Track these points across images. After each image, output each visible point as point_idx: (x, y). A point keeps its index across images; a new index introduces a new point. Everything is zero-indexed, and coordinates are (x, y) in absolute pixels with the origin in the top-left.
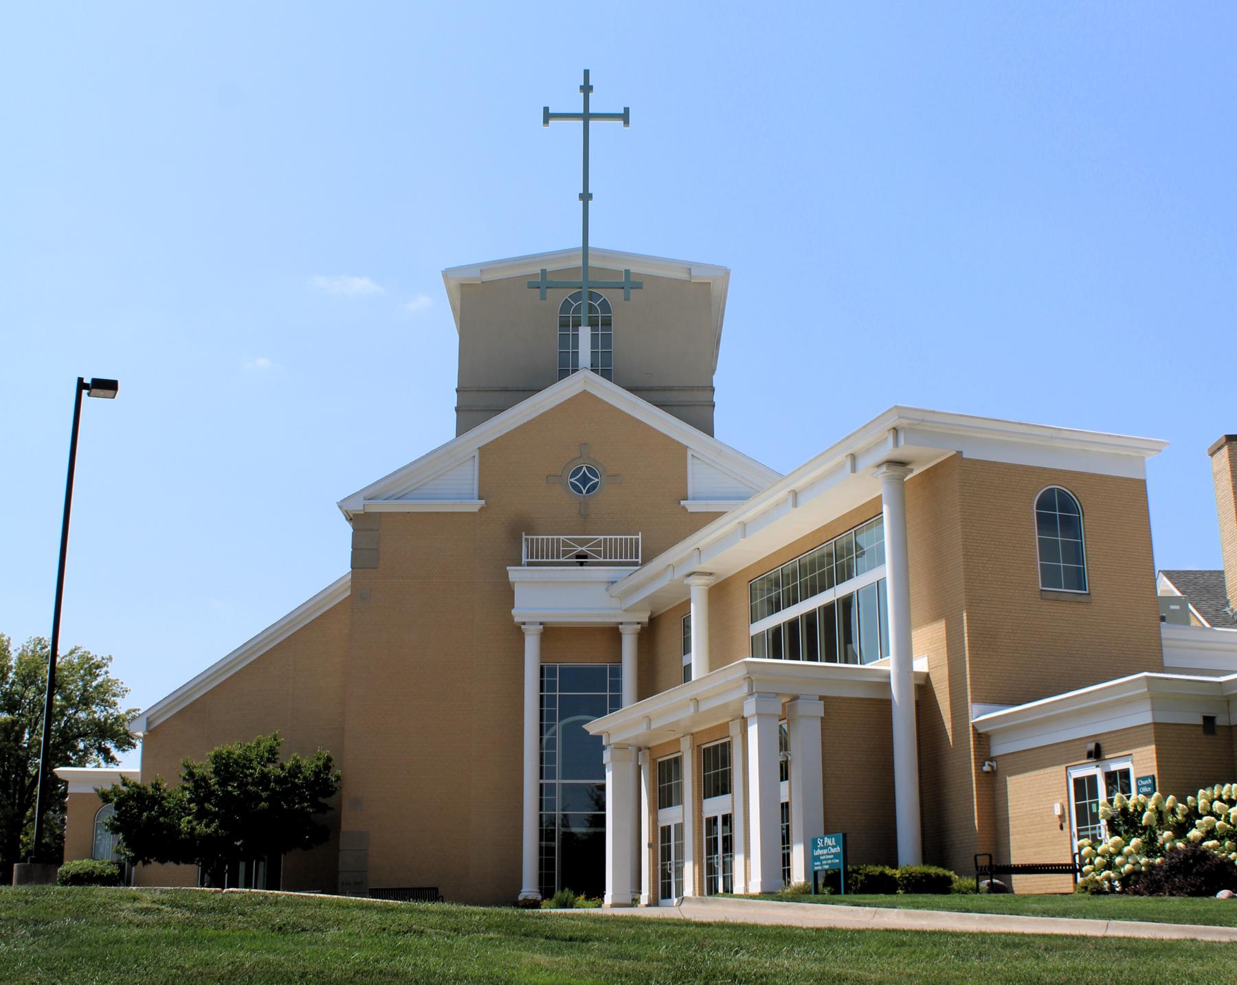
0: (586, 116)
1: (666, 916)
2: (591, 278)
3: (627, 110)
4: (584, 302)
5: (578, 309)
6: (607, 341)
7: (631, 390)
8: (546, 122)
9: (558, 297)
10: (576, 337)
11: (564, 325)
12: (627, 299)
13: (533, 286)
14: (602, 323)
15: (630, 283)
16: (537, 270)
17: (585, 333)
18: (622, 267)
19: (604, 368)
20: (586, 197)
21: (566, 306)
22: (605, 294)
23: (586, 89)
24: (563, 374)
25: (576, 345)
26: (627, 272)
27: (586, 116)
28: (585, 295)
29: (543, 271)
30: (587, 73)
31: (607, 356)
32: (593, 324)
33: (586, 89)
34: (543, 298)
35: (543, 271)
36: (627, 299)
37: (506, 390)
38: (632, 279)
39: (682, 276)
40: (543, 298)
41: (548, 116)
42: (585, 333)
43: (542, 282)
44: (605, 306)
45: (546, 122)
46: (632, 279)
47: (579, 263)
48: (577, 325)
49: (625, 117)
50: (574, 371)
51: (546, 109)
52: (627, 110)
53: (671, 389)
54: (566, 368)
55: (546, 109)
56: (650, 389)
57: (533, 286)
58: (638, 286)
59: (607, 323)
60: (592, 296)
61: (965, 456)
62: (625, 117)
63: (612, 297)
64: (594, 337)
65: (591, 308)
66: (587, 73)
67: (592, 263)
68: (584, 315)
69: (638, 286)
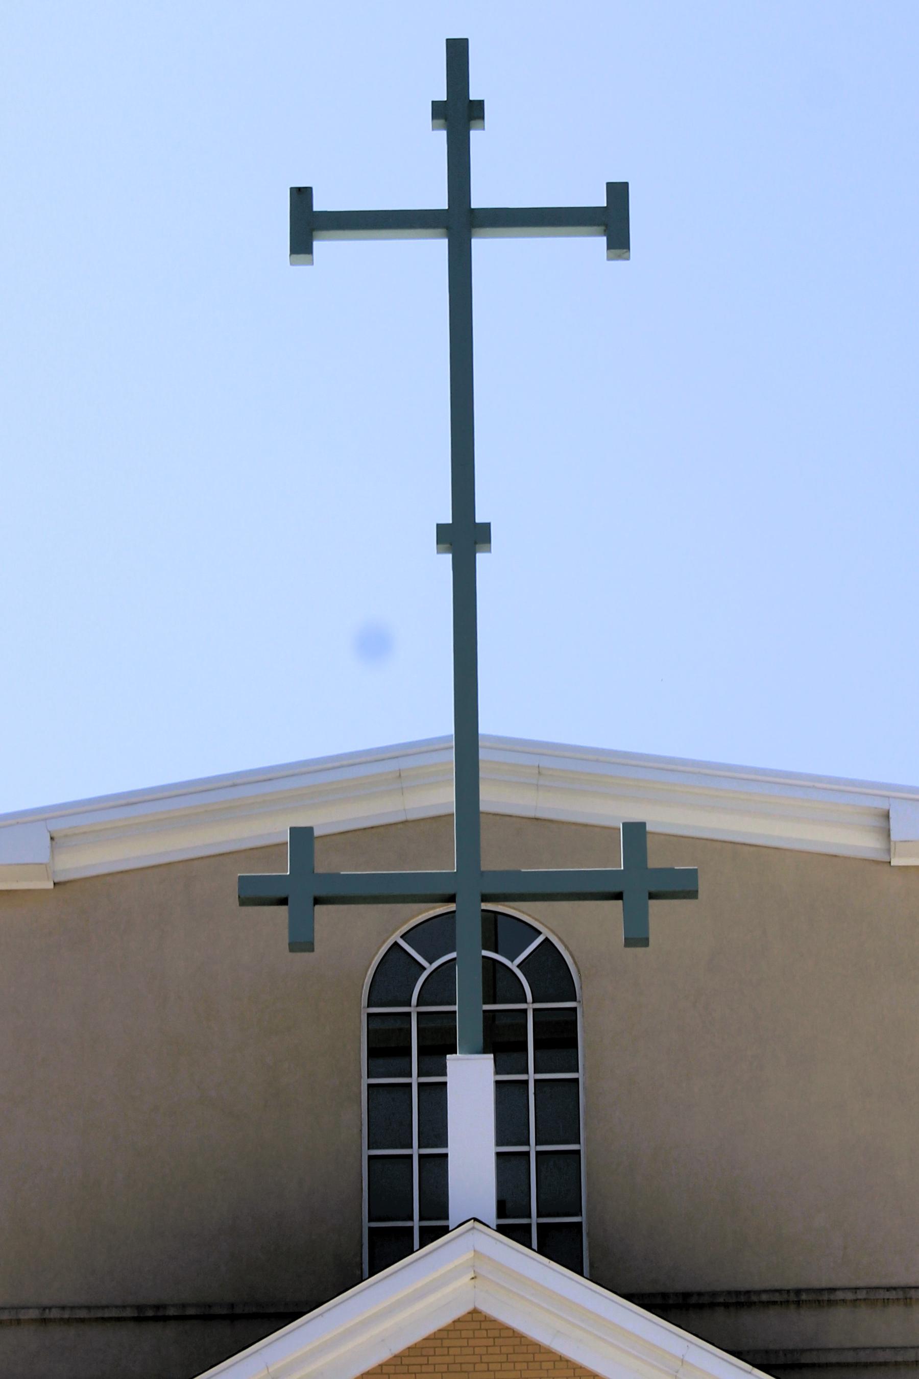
0: (460, 222)
1: (863, 1340)
2: (494, 859)
3: (618, 193)
4: (467, 956)
5: (441, 985)
6: (562, 1109)
7: (673, 1304)
8: (301, 245)
9: (361, 937)
10: (435, 1096)
11: (386, 1046)
12: (637, 939)
13: (257, 895)
14: (538, 1032)
15: (644, 878)
16: (275, 829)
17: (471, 1081)
18: (614, 813)
19: (549, 1215)
20: (464, 537)
21: (393, 972)
22: (547, 920)
23: (459, 114)
24: (390, 1247)
25: (435, 1130)
26: (635, 832)
27: (460, 222)
28: (469, 931)
29: (302, 837)
30: (457, 51)
31: (563, 1171)
32: (501, 1041)
33: (459, 114)
34: (302, 943)
35: (302, 837)
36: (637, 939)
37: (150, 1315)
38: (654, 862)
39: (859, 842)
40: (302, 943)
41: (308, 223)
42: (471, 1081)
43: (298, 883)
44: (551, 972)
45: (301, 245)
46: (654, 862)
47: (444, 798)
48: (439, 1045)
49: (611, 219)
50: (431, 1235)
51: (301, 197)
52: (618, 193)
53: (821, 1298)
54: (398, 1217)
55: (301, 197)
56: (742, 1301)
57: (257, 895)
58: (681, 887)
59: (560, 1037)
60: (495, 930)
61: (443, 97)
62: (611, 219)
63: (580, 932)
64: (508, 1096)
65: (495, 981)
66: (457, 51)
67: (492, 798)
68: (467, 1008)
69: (681, 887)
